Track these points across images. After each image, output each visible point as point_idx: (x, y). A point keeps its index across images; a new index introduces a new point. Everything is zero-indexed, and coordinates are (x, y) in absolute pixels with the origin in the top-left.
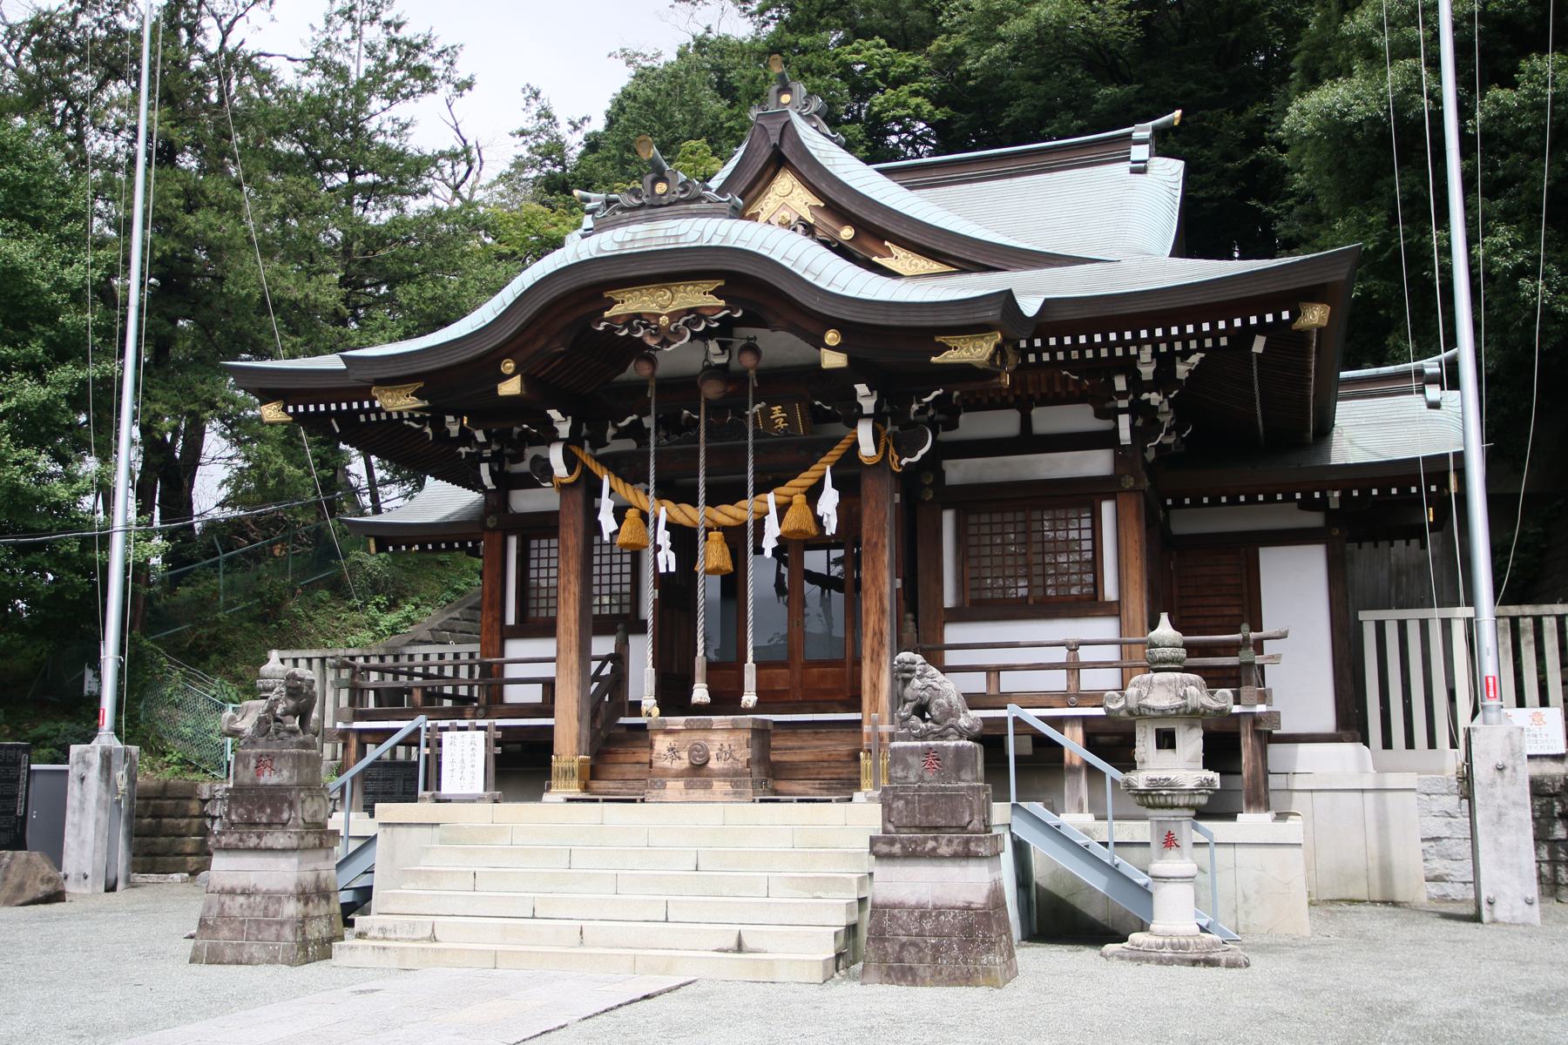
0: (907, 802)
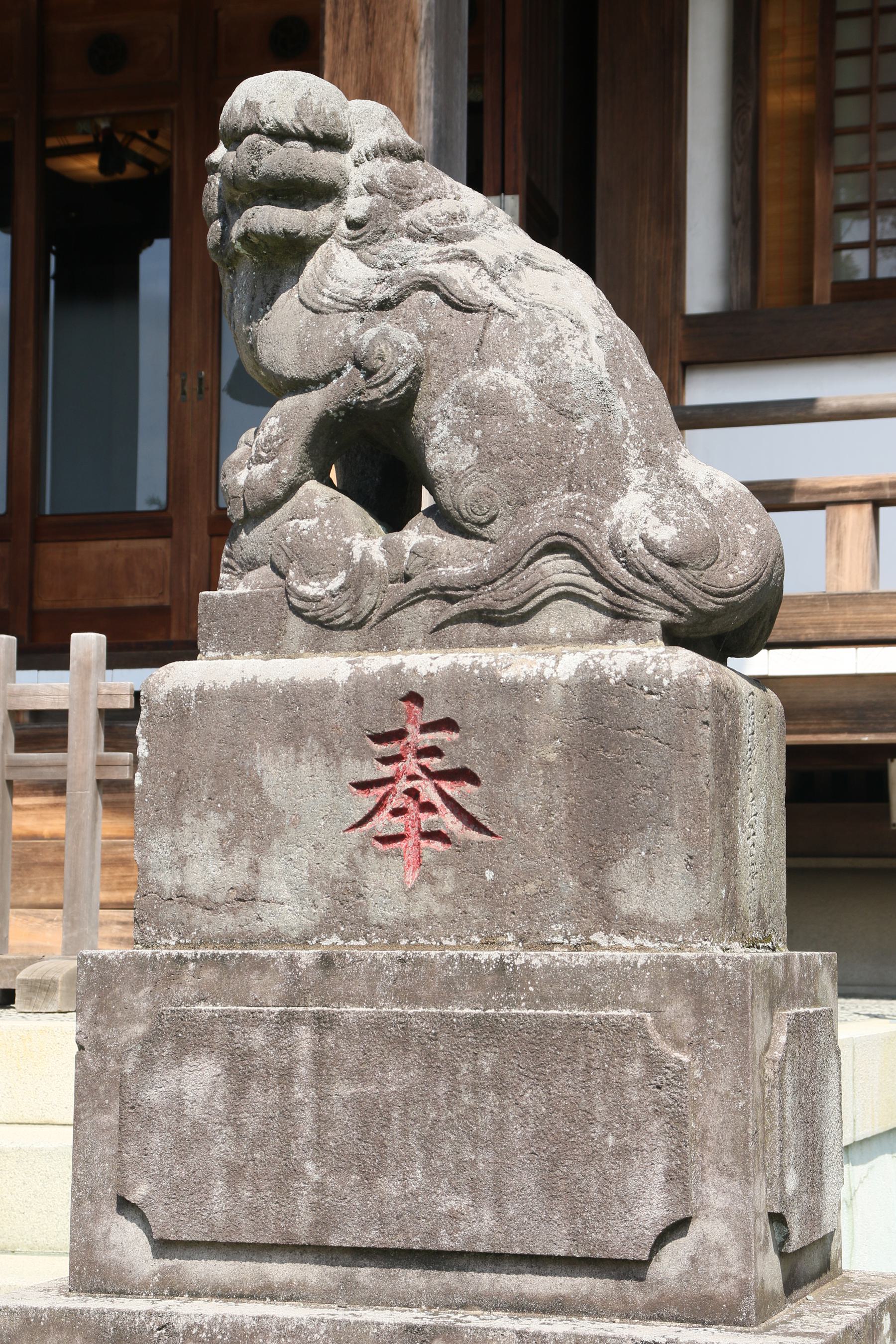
0: (240, 1070)
